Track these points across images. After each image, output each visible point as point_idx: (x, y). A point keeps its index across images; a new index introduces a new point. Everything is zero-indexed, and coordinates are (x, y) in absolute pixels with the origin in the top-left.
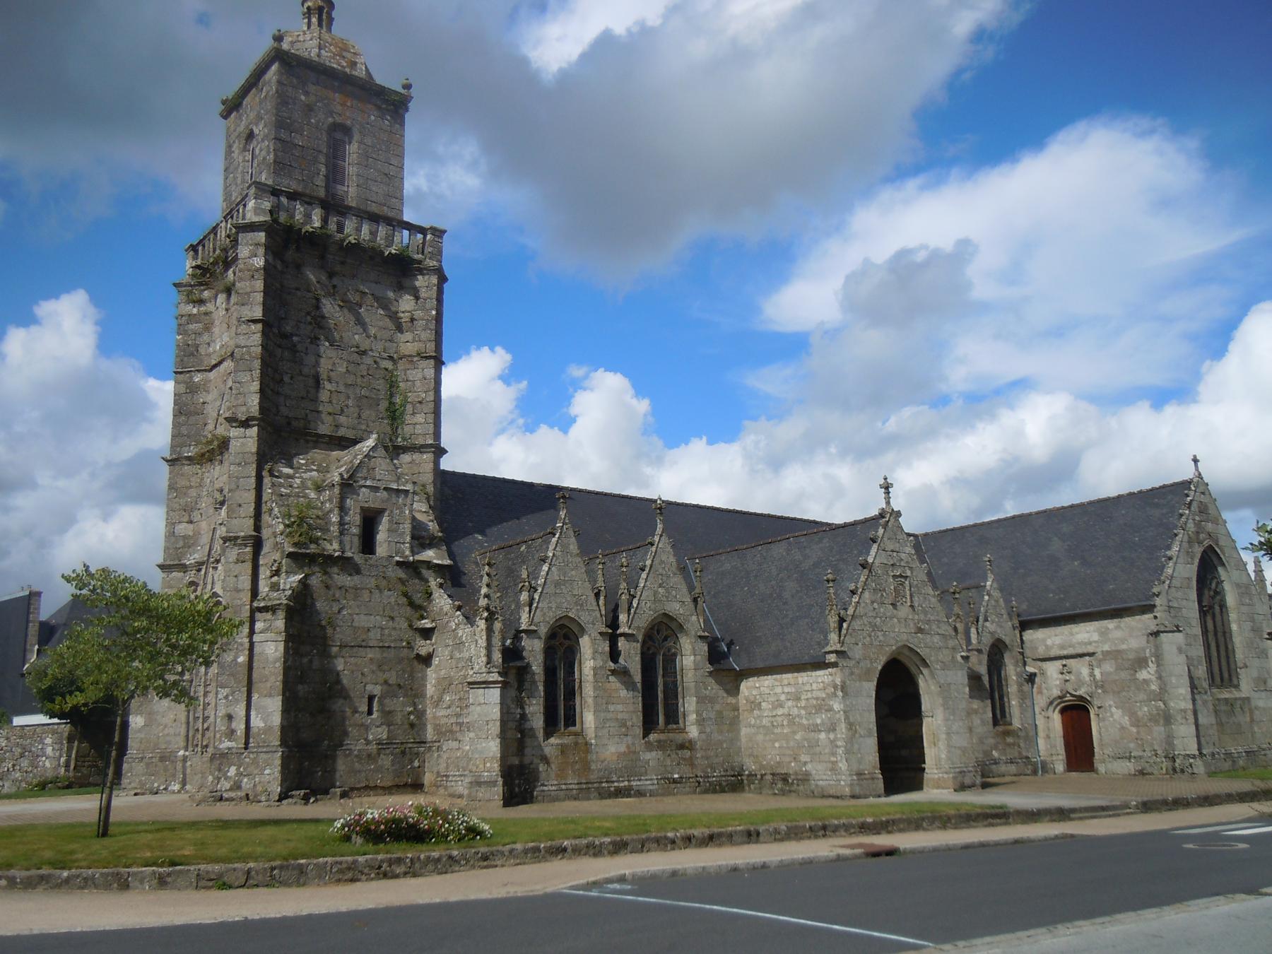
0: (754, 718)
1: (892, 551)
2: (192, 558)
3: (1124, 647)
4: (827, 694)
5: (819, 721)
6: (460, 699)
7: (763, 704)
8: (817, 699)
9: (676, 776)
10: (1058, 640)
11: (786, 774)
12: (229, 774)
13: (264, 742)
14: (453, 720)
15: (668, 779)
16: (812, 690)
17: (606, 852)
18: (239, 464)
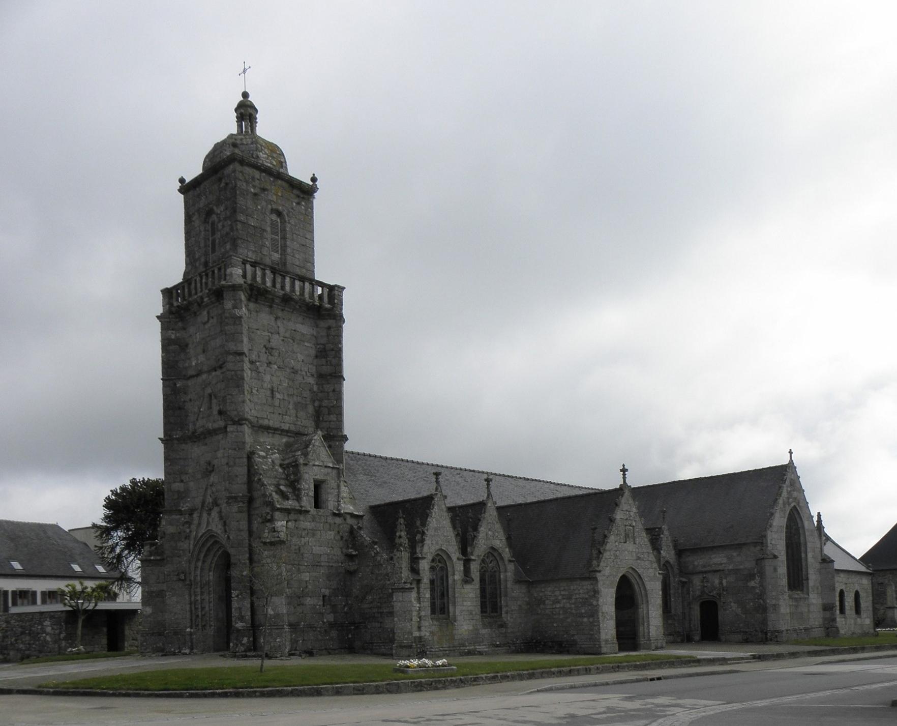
0: (540, 609)
1: (627, 511)
2: (184, 506)
3: (742, 567)
4: (589, 596)
5: (583, 611)
6: (380, 598)
7: (547, 602)
8: (582, 598)
9: (498, 643)
10: (701, 562)
11: (561, 641)
12: (243, 642)
13: (274, 623)
14: (376, 610)
15: (494, 645)
16: (580, 593)
17: (526, 678)
18: (235, 449)
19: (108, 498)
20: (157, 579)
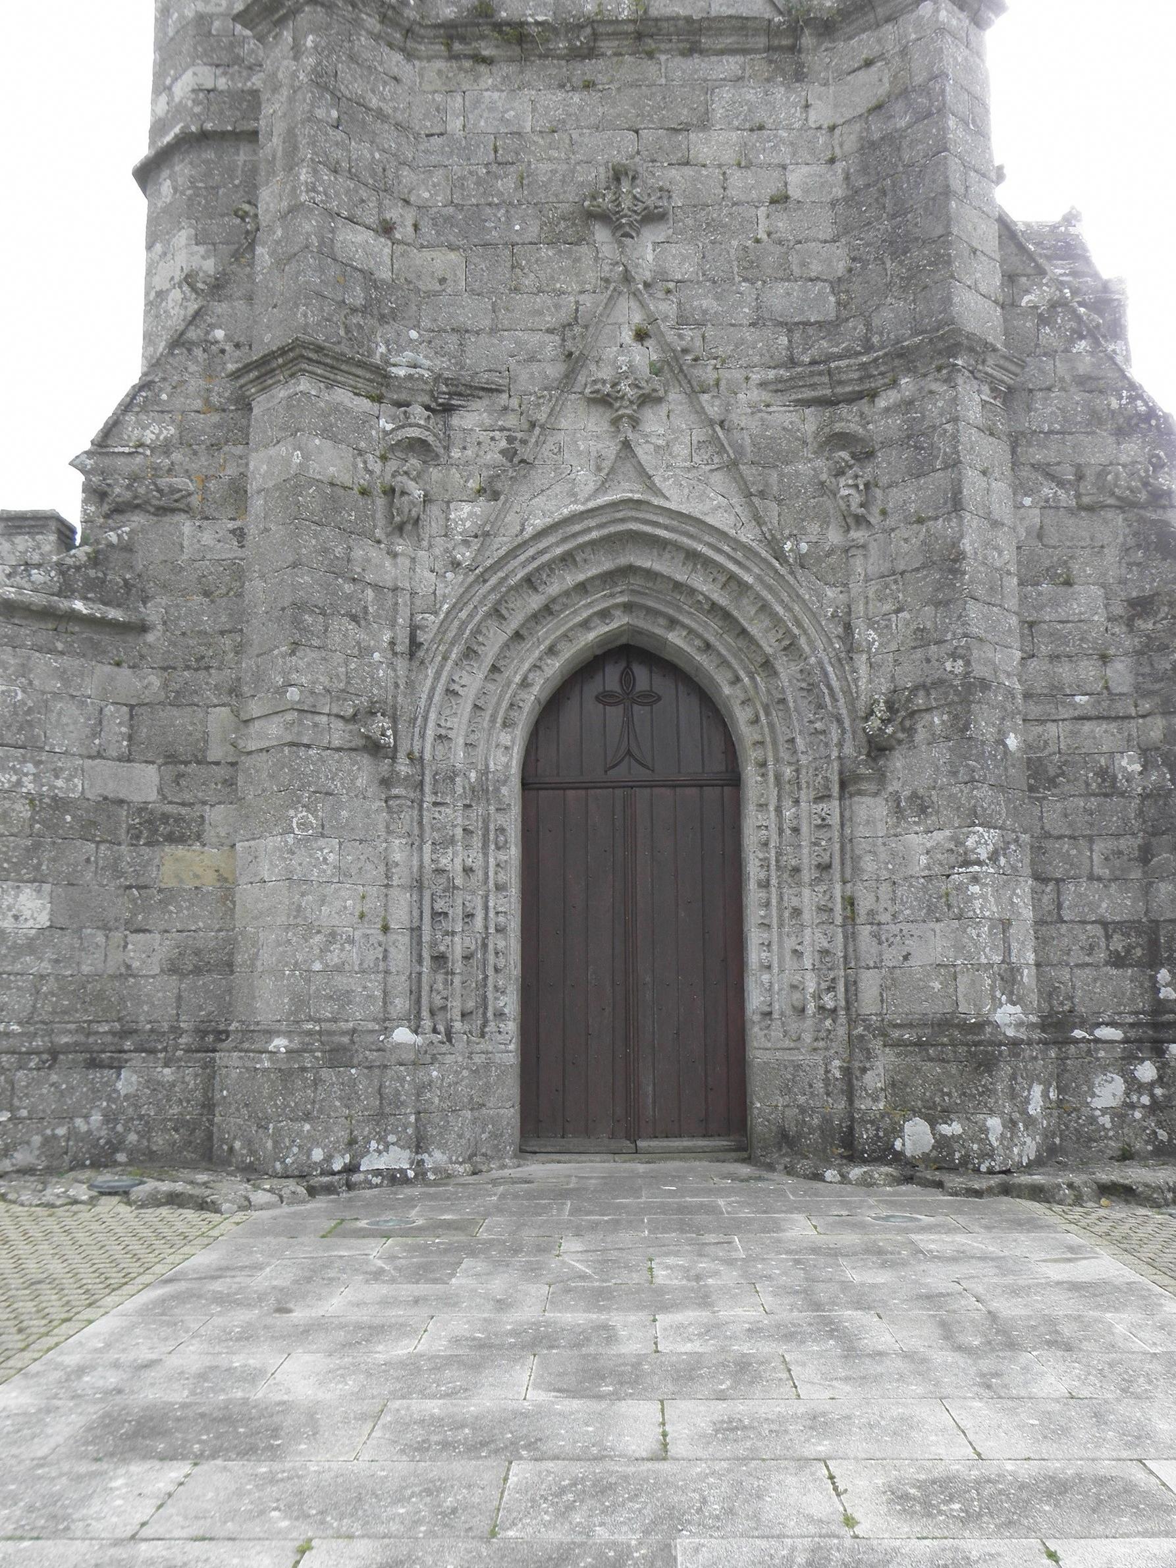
19: (997, 15)
20: (95, 735)
